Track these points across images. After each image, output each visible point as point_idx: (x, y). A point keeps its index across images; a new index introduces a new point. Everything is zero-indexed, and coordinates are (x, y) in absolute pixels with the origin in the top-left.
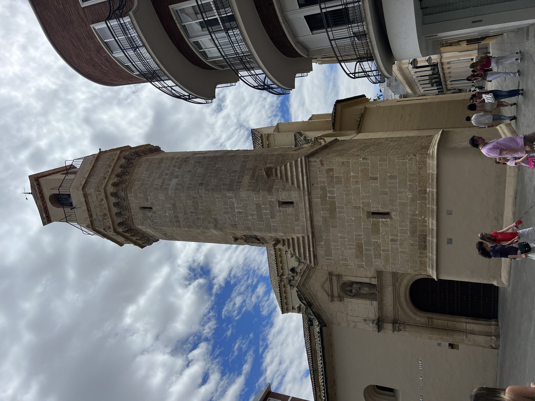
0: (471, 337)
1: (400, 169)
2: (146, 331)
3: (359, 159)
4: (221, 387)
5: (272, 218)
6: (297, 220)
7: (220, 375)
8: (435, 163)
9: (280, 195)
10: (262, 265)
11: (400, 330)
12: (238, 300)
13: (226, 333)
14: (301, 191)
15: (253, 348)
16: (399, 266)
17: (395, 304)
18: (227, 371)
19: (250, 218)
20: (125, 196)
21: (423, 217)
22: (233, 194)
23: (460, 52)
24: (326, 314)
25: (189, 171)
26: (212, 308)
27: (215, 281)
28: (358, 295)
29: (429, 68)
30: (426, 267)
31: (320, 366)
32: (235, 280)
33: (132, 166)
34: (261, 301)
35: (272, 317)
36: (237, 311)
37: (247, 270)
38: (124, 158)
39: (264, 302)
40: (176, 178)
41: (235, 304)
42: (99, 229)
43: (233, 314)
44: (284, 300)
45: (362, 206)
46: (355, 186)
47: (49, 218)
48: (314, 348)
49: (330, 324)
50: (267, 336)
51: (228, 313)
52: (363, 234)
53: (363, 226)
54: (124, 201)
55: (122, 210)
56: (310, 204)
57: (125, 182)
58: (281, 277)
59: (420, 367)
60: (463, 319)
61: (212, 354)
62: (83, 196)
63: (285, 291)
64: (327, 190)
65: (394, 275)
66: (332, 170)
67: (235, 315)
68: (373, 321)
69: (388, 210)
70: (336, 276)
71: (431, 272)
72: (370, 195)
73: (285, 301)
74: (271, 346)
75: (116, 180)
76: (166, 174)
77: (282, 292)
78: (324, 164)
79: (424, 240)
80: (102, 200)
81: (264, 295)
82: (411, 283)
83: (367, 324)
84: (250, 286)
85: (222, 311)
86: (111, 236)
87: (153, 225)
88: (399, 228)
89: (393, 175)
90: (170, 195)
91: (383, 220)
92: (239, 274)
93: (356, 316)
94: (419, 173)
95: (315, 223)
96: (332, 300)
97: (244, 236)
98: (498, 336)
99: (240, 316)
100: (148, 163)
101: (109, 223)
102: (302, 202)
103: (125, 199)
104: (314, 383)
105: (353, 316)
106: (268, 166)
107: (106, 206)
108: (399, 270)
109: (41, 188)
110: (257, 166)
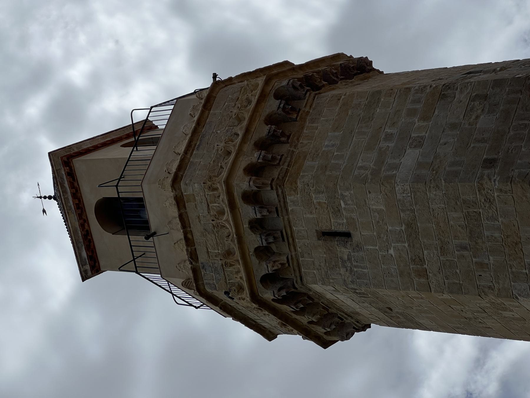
20: (280, 201)
25: (453, 126)
33: (297, 118)
38: (277, 96)
40: (415, 147)
42: (214, 291)
54: (278, 215)
57: (278, 162)
62: (174, 202)
76: (389, 137)
80: (222, 213)
87: (353, 282)
90: (399, 197)
103: (279, 209)
109: (76, 184)
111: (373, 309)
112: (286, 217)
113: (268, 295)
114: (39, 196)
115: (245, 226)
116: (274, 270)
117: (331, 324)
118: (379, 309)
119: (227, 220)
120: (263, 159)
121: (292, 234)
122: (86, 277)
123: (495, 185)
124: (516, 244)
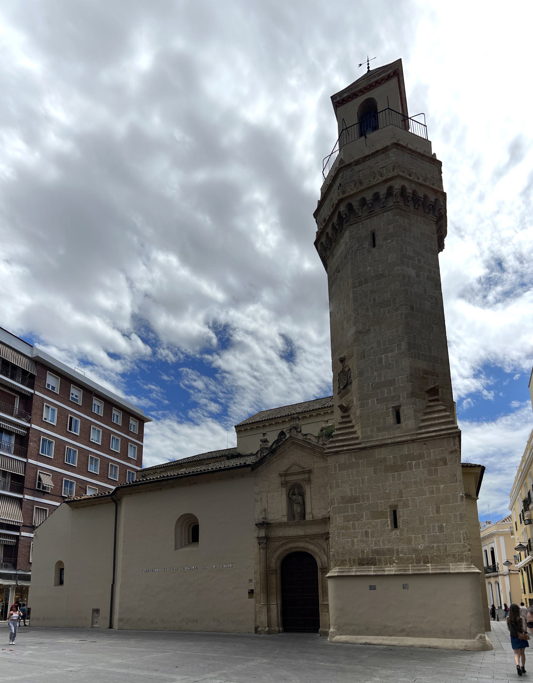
0: (265, 609)
1: (452, 535)
2: (152, 282)
3: (461, 493)
4: (109, 374)
5: (377, 400)
6: (379, 430)
7: (122, 372)
8: (464, 571)
9: (409, 407)
10: (239, 407)
11: (259, 544)
12: (199, 384)
13: (164, 375)
14: (416, 431)
15: (154, 405)
16: (336, 540)
17: (285, 538)
18: (127, 379)
19: (376, 374)
20: (388, 208)
21: (396, 561)
22: (405, 350)
23: (510, 593)
24: (265, 469)
25: (425, 291)
26: (187, 356)
27: (216, 357)
28: (290, 501)
29: (490, 563)
30: (338, 566)
31: (183, 471)
32: (220, 379)
33: (426, 212)
34: (202, 409)
35: (188, 422)
36: (188, 384)
37: (232, 390)
38: (436, 200)
39: (201, 413)
40: (416, 274)
41: (195, 381)
42: (340, 178)
43: (185, 380)
44: (249, 426)
45: (403, 500)
46: (427, 490)
47: (341, 103)
48: (204, 463)
49: (255, 475)
50: (168, 418)
51: (185, 374)
52: (370, 502)
53: (380, 503)
54: (382, 208)
55: (370, 206)
56: (374, 446)
57: (407, 204)
58: (297, 418)
59: (226, 566)
60: (279, 602)
61: (140, 361)
62: (385, 146)
63: (259, 427)
64: (420, 461)
65: (326, 536)
66: (445, 463)
67: (184, 383)
68: (265, 519)
69: (401, 527)
70: (309, 478)
71: (335, 571)
72: (418, 507)
73: (249, 428)
74: (159, 423)
75: (409, 191)
76: (419, 261)
77: (258, 424)
78: (452, 454)
79: (370, 562)
80: (382, 176)
81: (208, 412)
82: (310, 552)
83: (261, 513)
84: (217, 395)
85: (185, 367)
86: (329, 198)
87: (352, 251)
88: (382, 538)
89: (444, 529)
90: (395, 269)
91: (389, 523)
92: (226, 382)
93: (267, 501)
94: (449, 555)
95: (377, 451)
96: (281, 475)
97: (349, 370)
98: (269, 633)
99: (184, 388)
100: (430, 234)
101: (350, 191)
102: (402, 433)
103: (385, 208)
104: (168, 466)
105: (267, 498)
106: (440, 390)
107: (374, 182)
108: (332, 540)
109: (383, 82)
110: (438, 377)
111: (337, 264)
112: (380, 212)
113: (342, 208)
114: (369, 60)
115: (376, 190)
116: (355, 210)
117: (327, 244)
118: (338, 267)
119: (378, 179)
120: (409, 195)
123: (404, 311)
124: (379, 323)
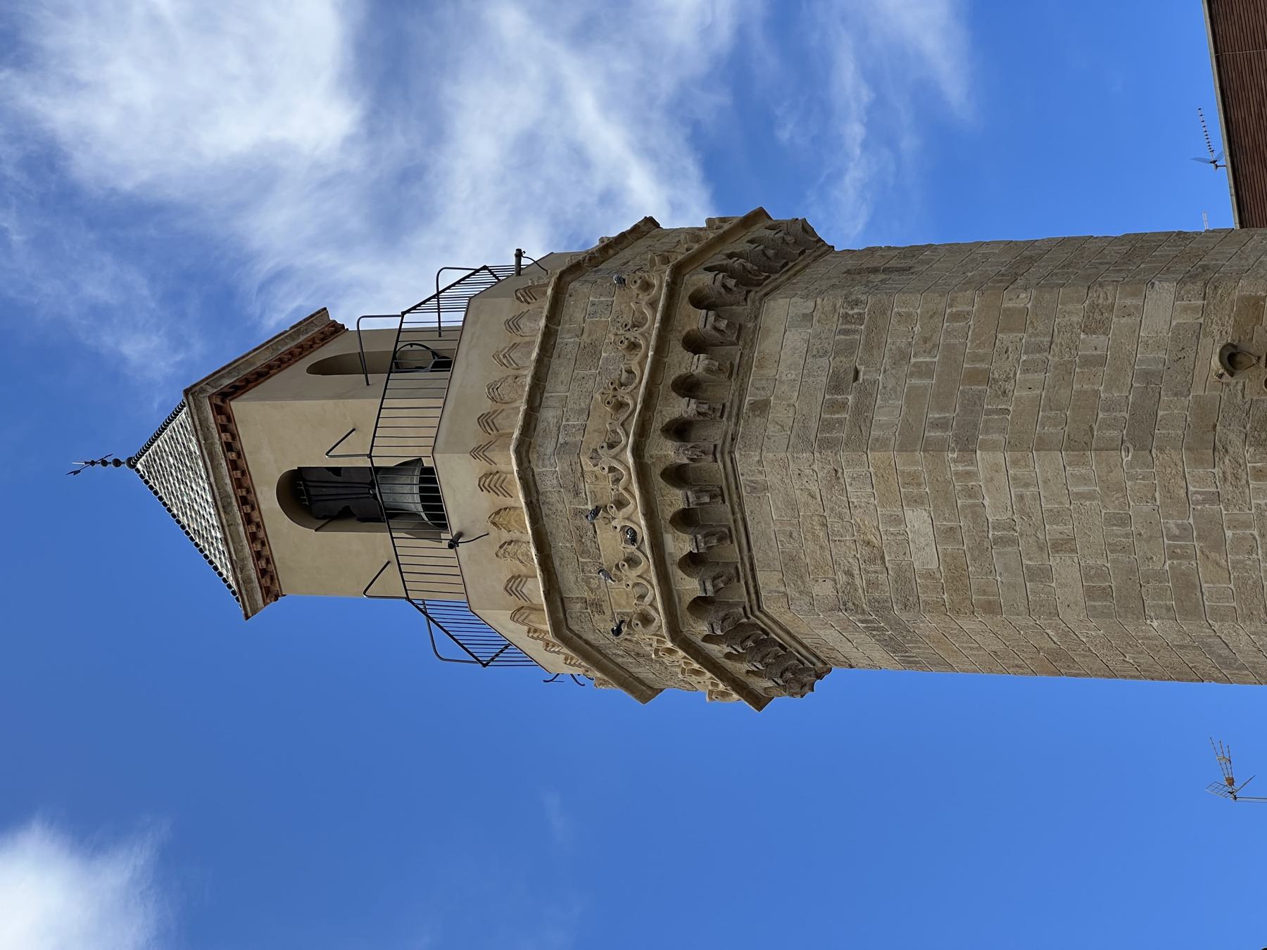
113: (699, 629)
121: (799, 271)
122: (194, 393)
